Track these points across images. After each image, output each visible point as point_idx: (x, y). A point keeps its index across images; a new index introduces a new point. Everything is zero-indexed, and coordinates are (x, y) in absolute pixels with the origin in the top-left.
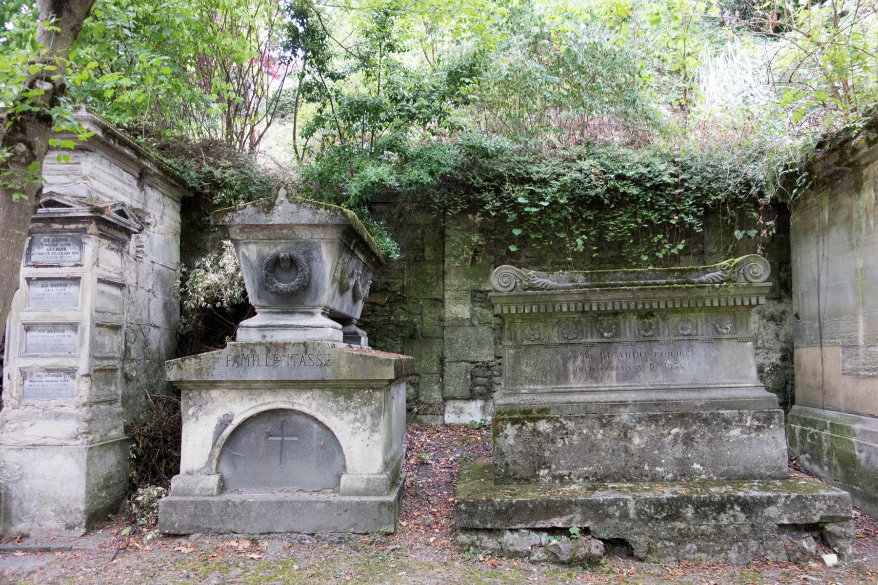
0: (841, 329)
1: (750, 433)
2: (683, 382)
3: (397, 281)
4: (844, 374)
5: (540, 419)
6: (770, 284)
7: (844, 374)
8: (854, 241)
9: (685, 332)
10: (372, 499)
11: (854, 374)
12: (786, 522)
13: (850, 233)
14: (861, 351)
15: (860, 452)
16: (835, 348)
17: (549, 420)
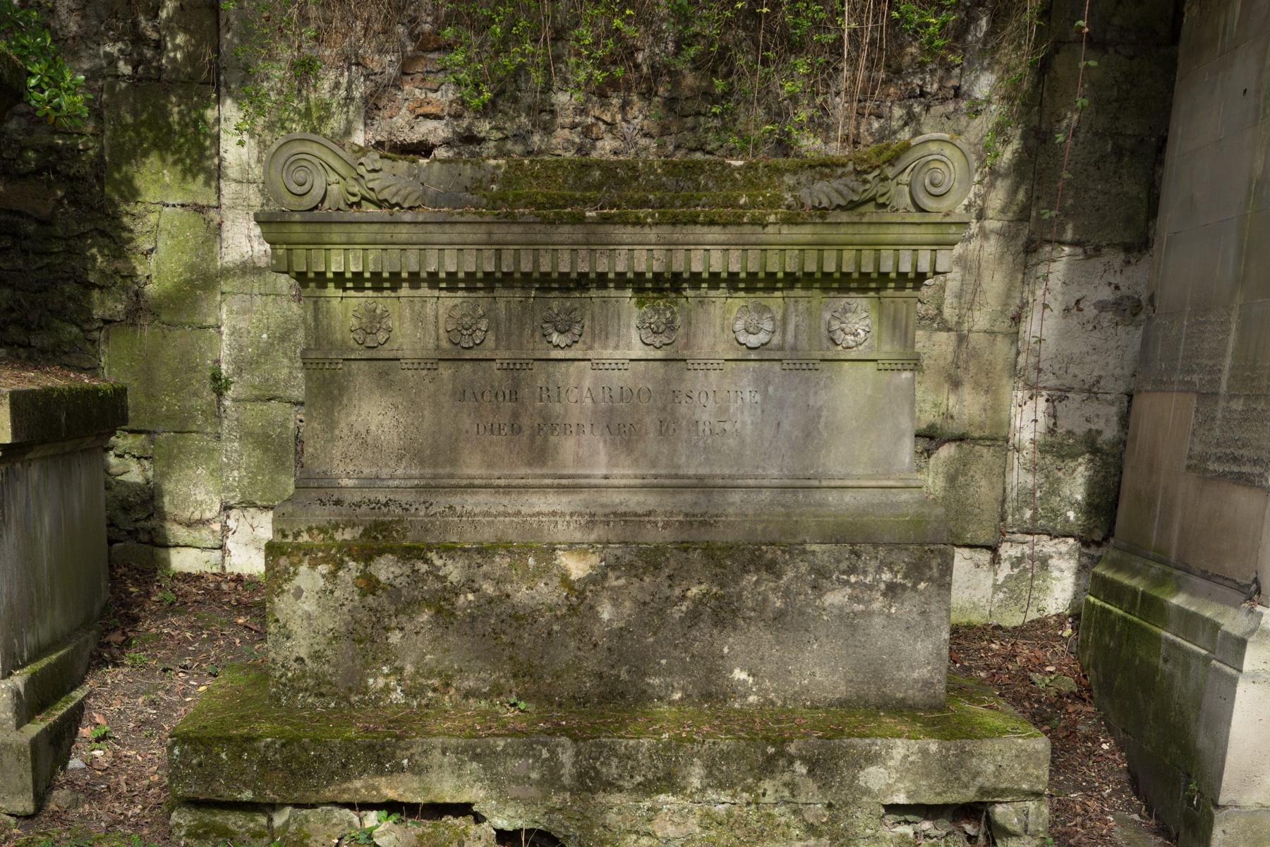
0: (1206, 346)
5: (380, 553)
11: (1197, 467)
12: (901, 799)
15: (1166, 661)
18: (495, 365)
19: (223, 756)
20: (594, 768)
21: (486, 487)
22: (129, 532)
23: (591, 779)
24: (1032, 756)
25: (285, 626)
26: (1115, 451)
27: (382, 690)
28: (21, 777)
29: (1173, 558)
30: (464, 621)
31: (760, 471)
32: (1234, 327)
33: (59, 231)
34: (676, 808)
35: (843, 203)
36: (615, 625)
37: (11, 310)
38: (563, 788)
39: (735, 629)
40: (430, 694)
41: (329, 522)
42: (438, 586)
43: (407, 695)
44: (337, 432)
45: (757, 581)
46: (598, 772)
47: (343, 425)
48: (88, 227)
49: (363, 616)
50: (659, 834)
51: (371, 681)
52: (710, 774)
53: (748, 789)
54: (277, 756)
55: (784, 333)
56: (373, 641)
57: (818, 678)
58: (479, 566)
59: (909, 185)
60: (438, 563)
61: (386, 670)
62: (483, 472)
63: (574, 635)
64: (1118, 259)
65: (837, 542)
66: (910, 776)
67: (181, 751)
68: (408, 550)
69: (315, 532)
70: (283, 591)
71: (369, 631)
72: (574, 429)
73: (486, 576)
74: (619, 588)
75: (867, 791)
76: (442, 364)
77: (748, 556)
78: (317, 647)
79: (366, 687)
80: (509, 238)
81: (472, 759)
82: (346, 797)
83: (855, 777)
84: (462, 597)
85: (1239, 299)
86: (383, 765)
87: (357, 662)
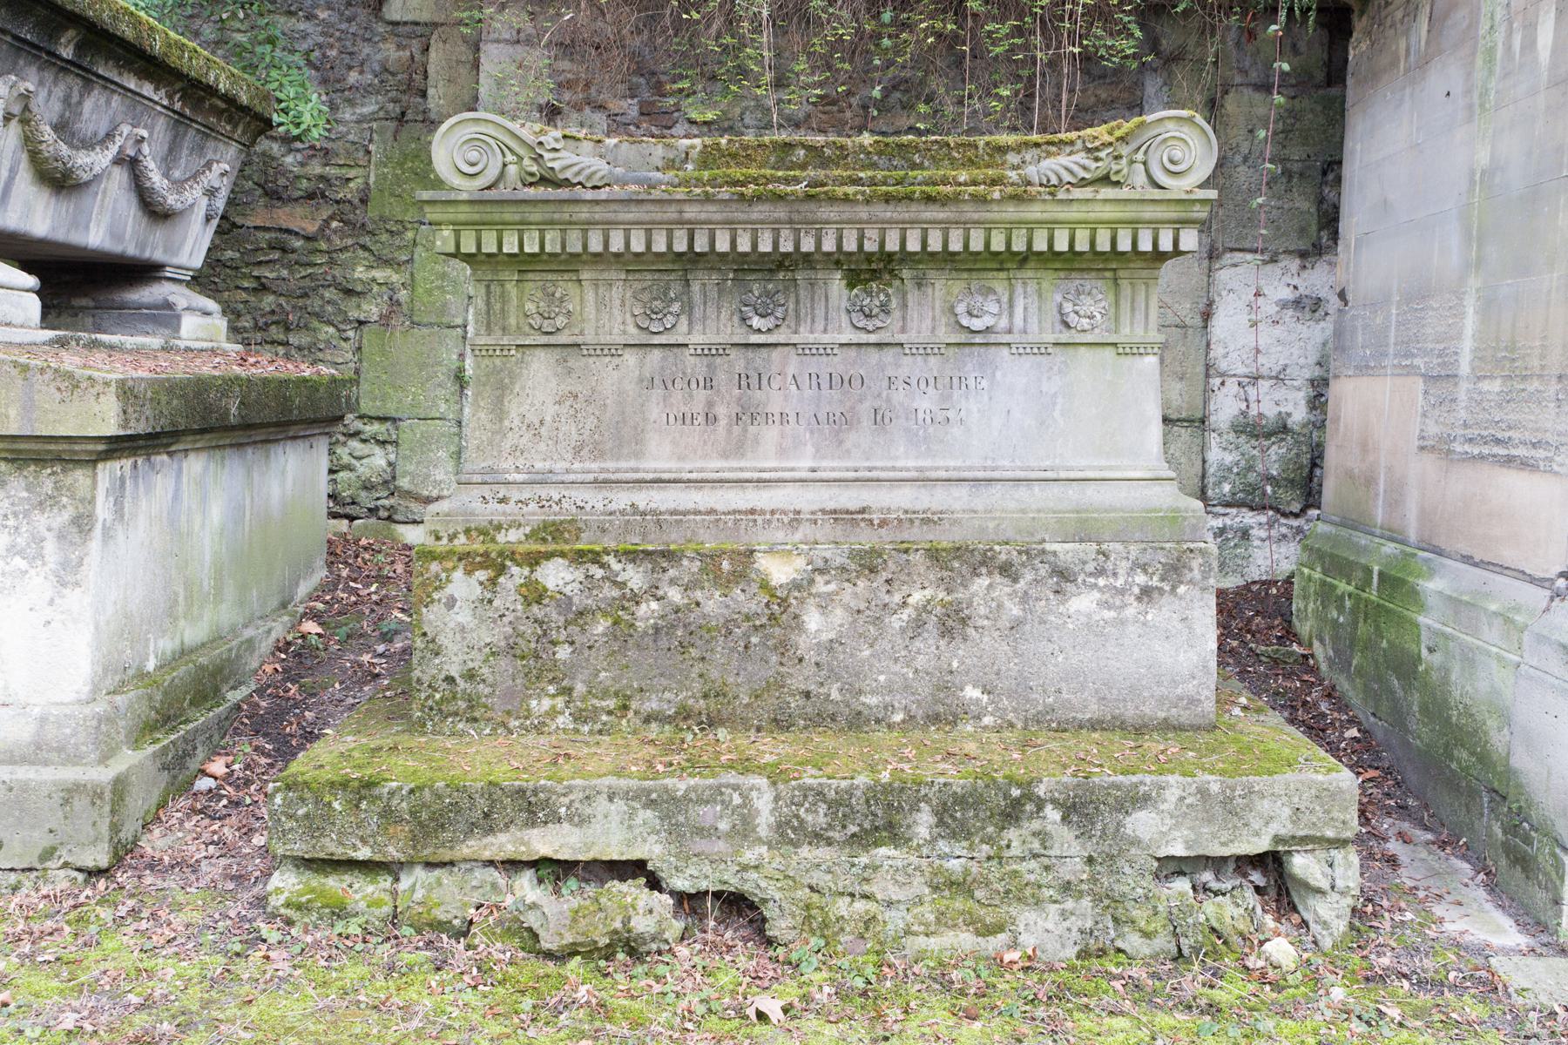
0: (1429, 330)
1: (1124, 606)
2: (972, 460)
3: (351, 173)
4: (1422, 448)
5: (549, 556)
6: (1212, 194)
7: (1422, 448)
8: (1476, 95)
9: (977, 324)
10: (48, 774)
11: (1438, 448)
12: (1179, 850)
13: (1469, 74)
14: (1463, 391)
15: (1431, 650)
16: (1410, 379)
17: (579, 557)
18: (687, 352)
19: (336, 805)
20: (797, 816)
21: (675, 481)
22: (370, 510)
23: (794, 829)
24: (1335, 794)
25: (433, 641)
26: (1305, 431)
27: (547, 713)
28: (94, 824)
29: (1413, 537)
30: (645, 633)
31: (989, 463)
32: (1470, 311)
33: (324, 246)
34: (900, 864)
35: (1073, 181)
36: (825, 637)
37: (273, 312)
38: (760, 840)
39: (965, 640)
40: (604, 718)
41: (491, 522)
42: (616, 593)
43: (575, 720)
44: (506, 423)
45: (990, 585)
46: (802, 822)
47: (513, 414)
48: (350, 242)
49: (528, 629)
50: (879, 897)
51: (534, 703)
52: (941, 823)
53: (988, 840)
54: (404, 804)
55: (1011, 315)
56: (537, 657)
57: (1065, 695)
58: (664, 571)
59: (1145, 163)
60: (616, 566)
61: (551, 689)
62: (673, 465)
63: (776, 648)
64: (1294, 264)
65: (1081, 541)
66: (1188, 823)
67: (284, 799)
68: (581, 553)
69: (474, 534)
70: (432, 601)
71: (533, 645)
72: (777, 418)
73: (672, 582)
74: (829, 594)
75: (1135, 842)
76: (628, 350)
77: (979, 558)
78: (471, 665)
79: (528, 710)
80: (703, 216)
81: (646, 806)
82: (487, 855)
83: (1119, 824)
84: (643, 606)
85: (1474, 282)
86: (534, 813)
87: (518, 681)
